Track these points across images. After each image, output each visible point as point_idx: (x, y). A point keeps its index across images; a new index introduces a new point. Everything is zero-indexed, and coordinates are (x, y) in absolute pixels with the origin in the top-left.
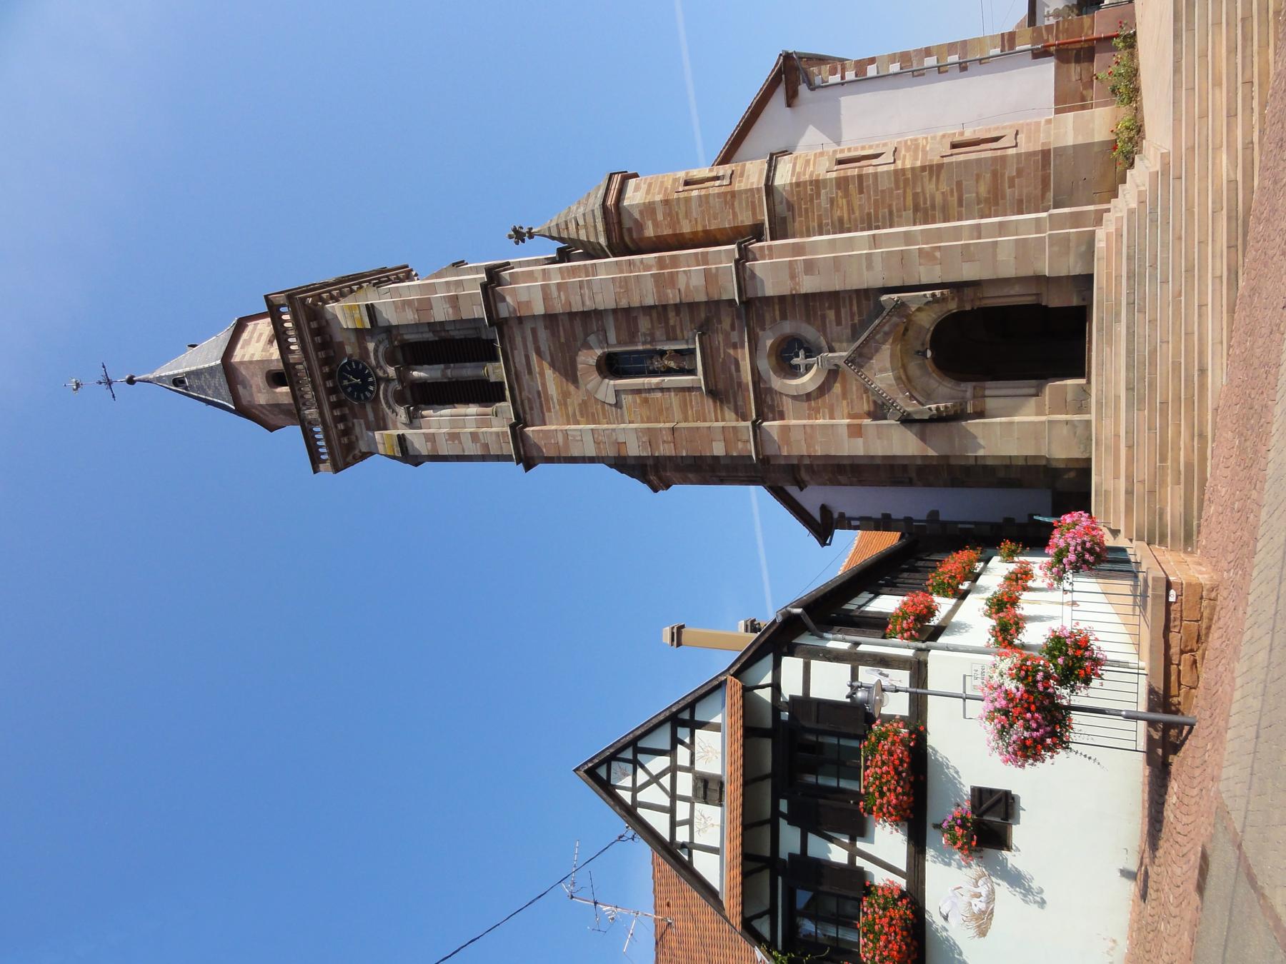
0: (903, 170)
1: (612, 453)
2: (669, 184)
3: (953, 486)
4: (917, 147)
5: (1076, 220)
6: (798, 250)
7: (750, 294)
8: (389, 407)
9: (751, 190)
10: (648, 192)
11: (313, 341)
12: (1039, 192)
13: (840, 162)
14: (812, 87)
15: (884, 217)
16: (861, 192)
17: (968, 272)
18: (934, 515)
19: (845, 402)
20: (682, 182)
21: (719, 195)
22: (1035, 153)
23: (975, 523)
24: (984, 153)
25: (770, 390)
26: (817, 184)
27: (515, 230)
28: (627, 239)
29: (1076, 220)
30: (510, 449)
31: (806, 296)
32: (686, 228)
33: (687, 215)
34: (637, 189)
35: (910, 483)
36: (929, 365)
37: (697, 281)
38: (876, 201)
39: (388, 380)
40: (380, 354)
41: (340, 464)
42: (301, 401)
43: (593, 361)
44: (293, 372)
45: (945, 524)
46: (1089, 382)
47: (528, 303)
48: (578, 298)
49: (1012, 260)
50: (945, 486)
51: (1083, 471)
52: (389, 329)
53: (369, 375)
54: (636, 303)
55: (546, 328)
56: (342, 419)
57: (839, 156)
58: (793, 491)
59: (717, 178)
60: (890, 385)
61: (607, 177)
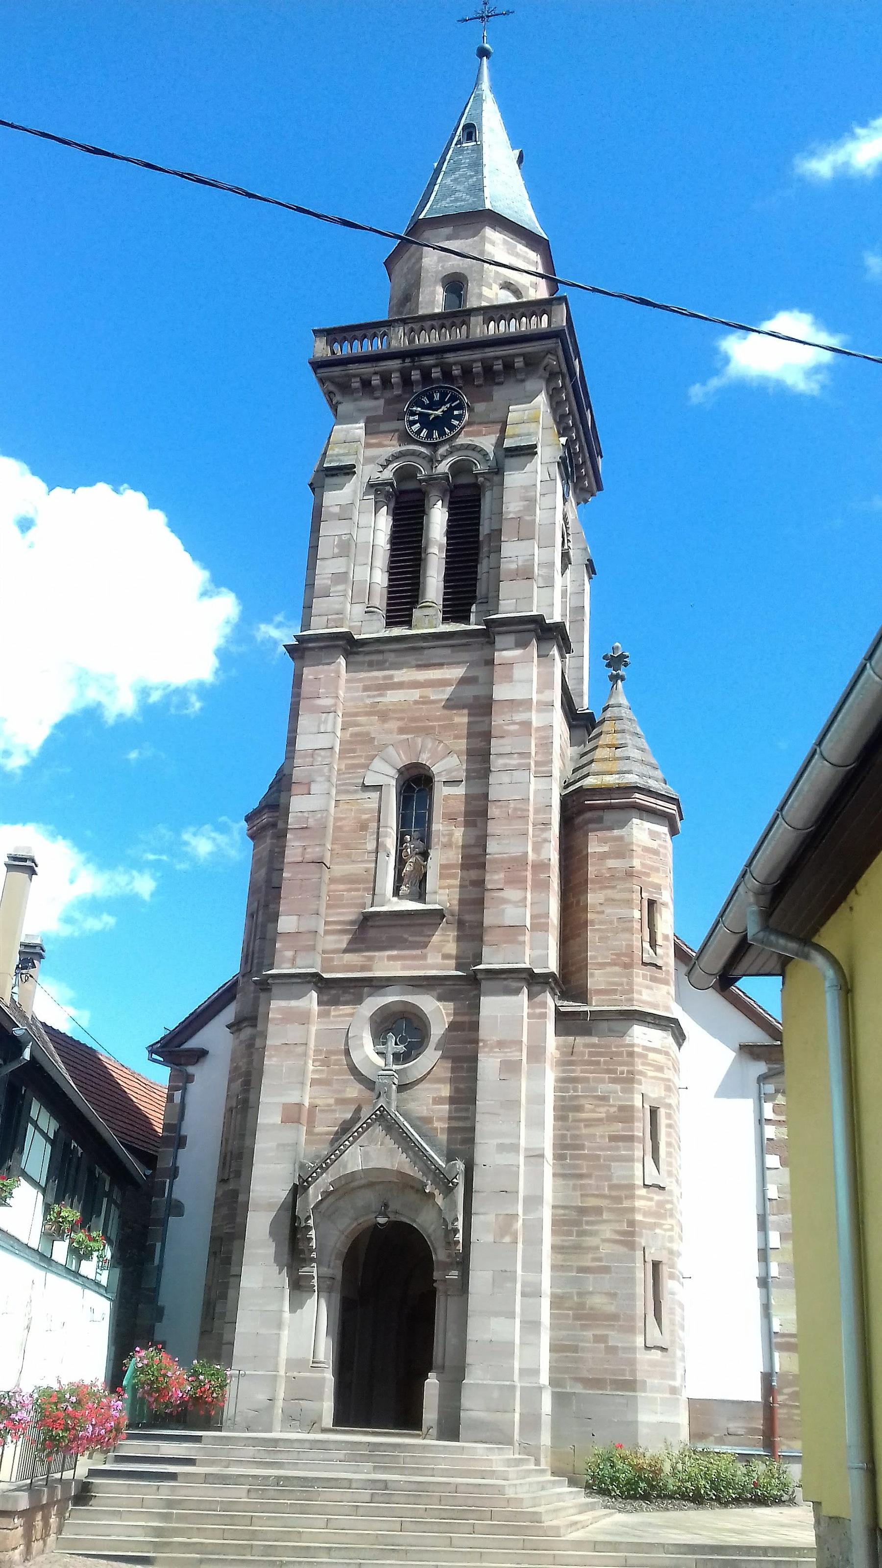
0: (632, 1197)
1: (298, 774)
2: (654, 879)
3: (213, 1239)
4: (662, 1216)
5: (531, 1422)
6: (537, 1053)
7: (485, 985)
8: (395, 457)
9: (631, 991)
10: (646, 849)
11: (497, 358)
12: (586, 1374)
13: (654, 1112)
14: (763, 1079)
15: (575, 1167)
16: (613, 1138)
17: (480, 1278)
18: (177, 1209)
19: (331, 1101)
20: (654, 897)
21: (631, 946)
22: (633, 1372)
23: (160, 1268)
24: (642, 1303)
25: (358, 1000)
26: (629, 1080)
27: (622, 657)
28: (589, 815)
29: (531, 1422)
30: (318, 628)
31: (475, 1059)
32: (593, 898)
33: (610, 901)
34: (654, 835)
35: (222, 1181)
36: (368, 1219)
37: (510, 915)
38: (598, 1157)
39: (432, 461)
40: (470, 453)
41: (325, 372)
42: (416, 326)
43: (424, 759)
44: (458, 321)
45: (164, 1223)
46: (325, 1431)
47: (509, 679)
48: (508, 750)
49: (487, 1337)
50: (213, 1229)
51: (408, 1418)
52: (498, 471)
53: (442, 433)
54: (492, 827)
55: (476, 698)
56: (386, 382)
57: (662, 1112)
58: (229, 1014)
59: (653, 944)
60: (345, 1167)
61: (674, 794)
